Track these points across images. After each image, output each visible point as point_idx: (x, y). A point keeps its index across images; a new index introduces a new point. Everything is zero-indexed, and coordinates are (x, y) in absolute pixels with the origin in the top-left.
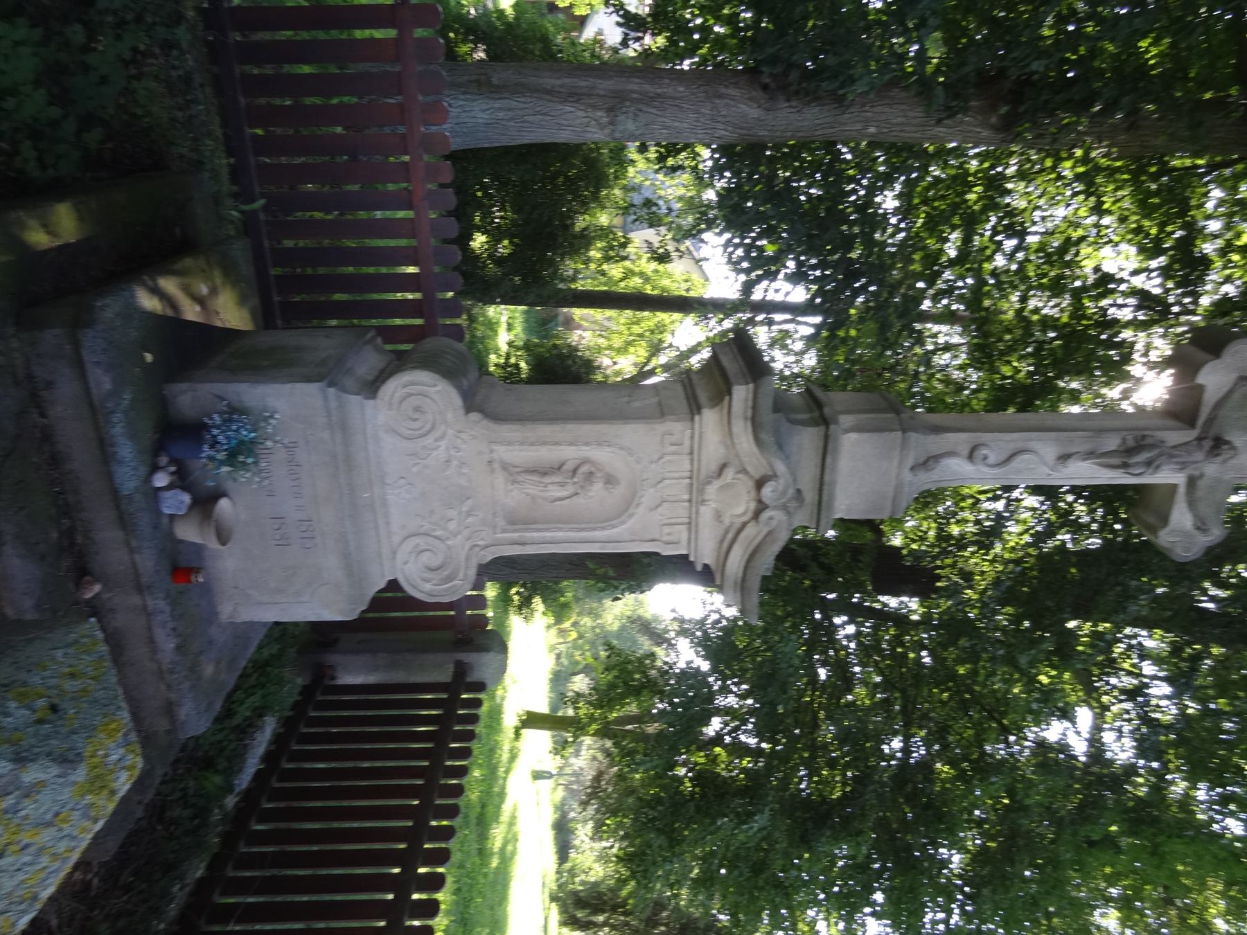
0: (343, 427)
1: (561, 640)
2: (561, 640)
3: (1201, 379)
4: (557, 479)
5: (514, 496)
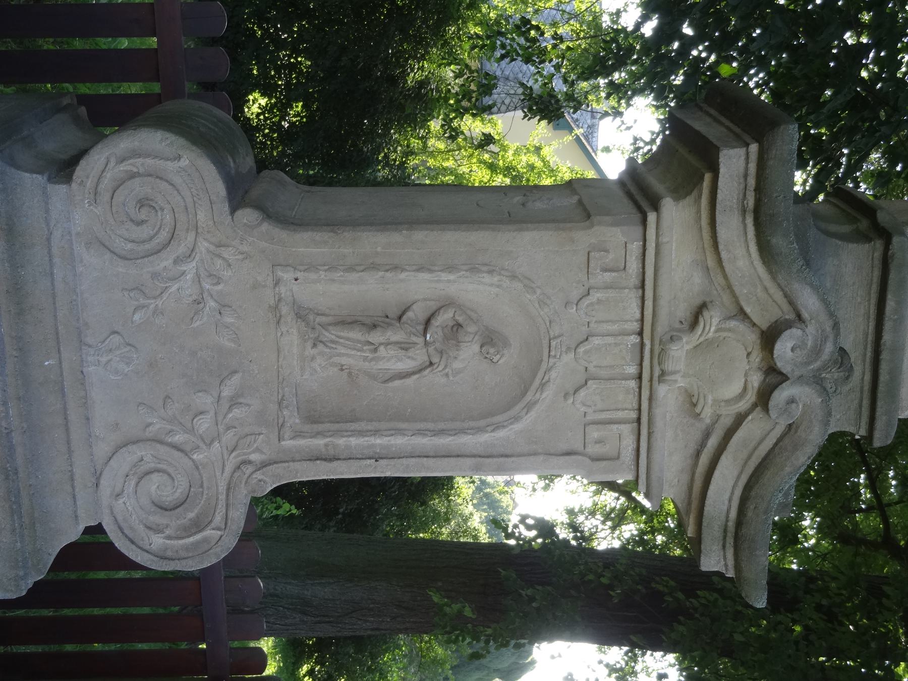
4: (396, 335)
5: (316, 370)
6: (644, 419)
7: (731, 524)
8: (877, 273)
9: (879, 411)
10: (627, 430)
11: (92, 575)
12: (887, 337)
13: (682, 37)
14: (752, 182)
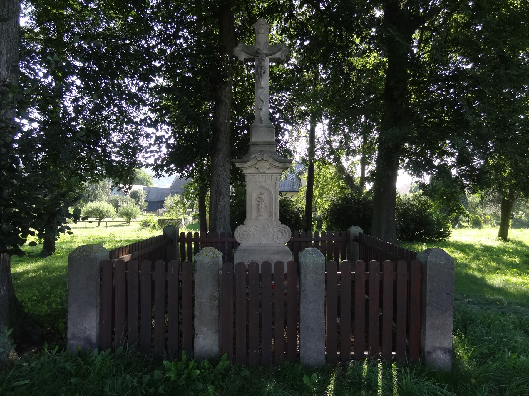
0: (245, 250)
1: (490, 222)
2: (490, 222)
3: (243, 60)
4: (260, 205)
5: (265, 216)
13: (126, 40)
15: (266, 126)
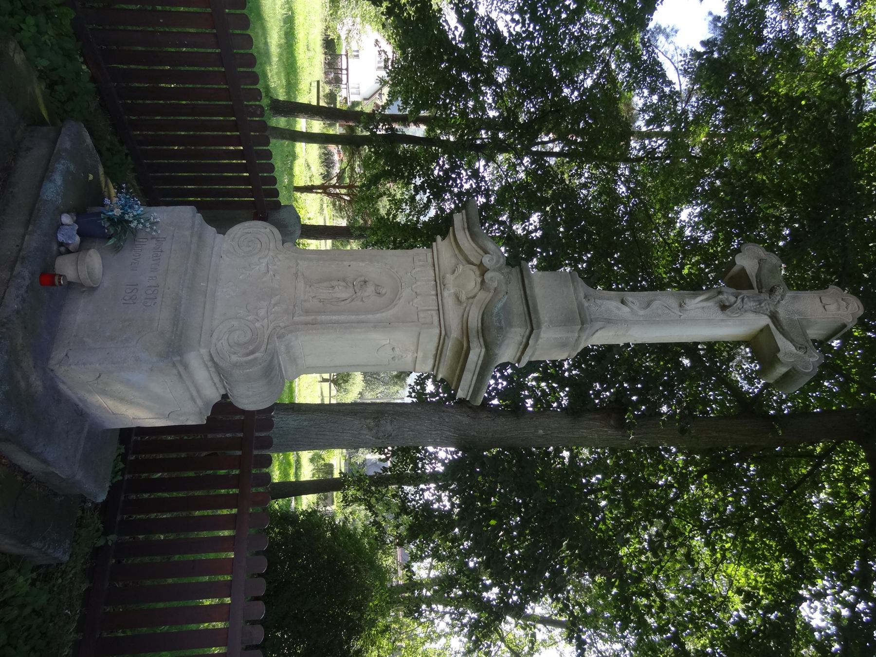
6: (441, 307)
7: (480, 328)
8: (519, 276)
9: (533, 318)
10: (434, 313)
11: (220, 512)
12: (528, 292)
14: (465, 220)
15: (580, 307)
